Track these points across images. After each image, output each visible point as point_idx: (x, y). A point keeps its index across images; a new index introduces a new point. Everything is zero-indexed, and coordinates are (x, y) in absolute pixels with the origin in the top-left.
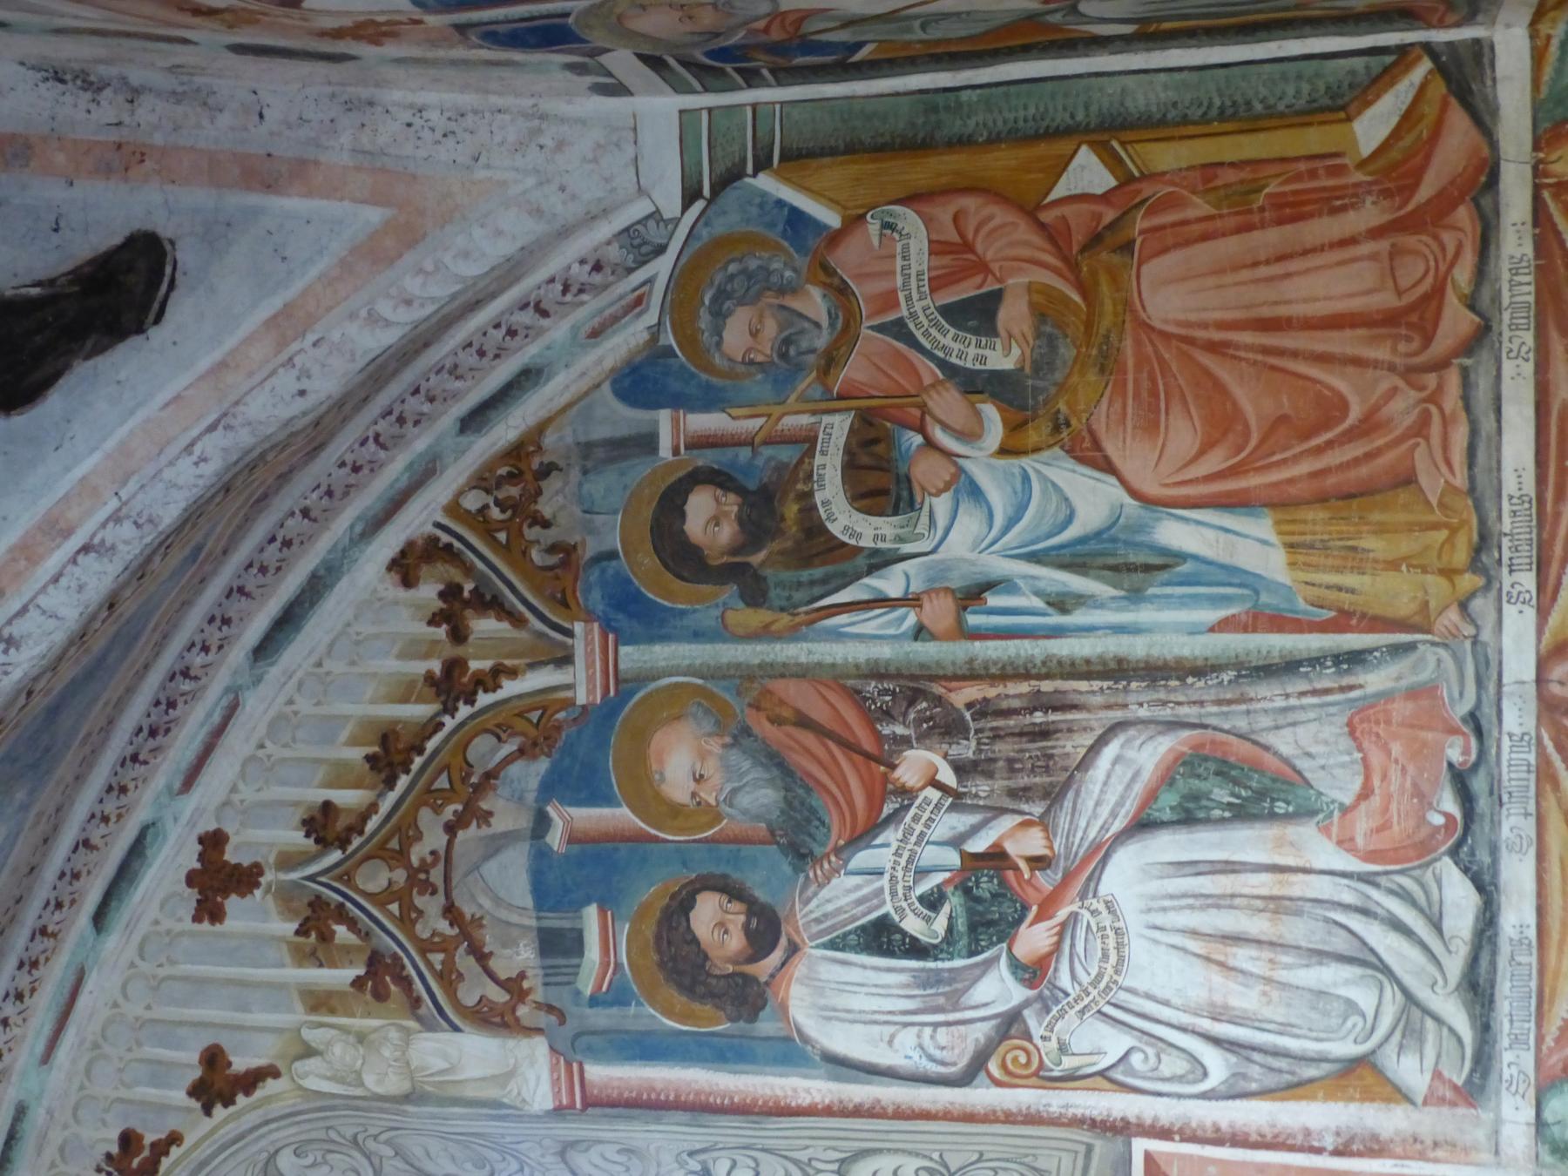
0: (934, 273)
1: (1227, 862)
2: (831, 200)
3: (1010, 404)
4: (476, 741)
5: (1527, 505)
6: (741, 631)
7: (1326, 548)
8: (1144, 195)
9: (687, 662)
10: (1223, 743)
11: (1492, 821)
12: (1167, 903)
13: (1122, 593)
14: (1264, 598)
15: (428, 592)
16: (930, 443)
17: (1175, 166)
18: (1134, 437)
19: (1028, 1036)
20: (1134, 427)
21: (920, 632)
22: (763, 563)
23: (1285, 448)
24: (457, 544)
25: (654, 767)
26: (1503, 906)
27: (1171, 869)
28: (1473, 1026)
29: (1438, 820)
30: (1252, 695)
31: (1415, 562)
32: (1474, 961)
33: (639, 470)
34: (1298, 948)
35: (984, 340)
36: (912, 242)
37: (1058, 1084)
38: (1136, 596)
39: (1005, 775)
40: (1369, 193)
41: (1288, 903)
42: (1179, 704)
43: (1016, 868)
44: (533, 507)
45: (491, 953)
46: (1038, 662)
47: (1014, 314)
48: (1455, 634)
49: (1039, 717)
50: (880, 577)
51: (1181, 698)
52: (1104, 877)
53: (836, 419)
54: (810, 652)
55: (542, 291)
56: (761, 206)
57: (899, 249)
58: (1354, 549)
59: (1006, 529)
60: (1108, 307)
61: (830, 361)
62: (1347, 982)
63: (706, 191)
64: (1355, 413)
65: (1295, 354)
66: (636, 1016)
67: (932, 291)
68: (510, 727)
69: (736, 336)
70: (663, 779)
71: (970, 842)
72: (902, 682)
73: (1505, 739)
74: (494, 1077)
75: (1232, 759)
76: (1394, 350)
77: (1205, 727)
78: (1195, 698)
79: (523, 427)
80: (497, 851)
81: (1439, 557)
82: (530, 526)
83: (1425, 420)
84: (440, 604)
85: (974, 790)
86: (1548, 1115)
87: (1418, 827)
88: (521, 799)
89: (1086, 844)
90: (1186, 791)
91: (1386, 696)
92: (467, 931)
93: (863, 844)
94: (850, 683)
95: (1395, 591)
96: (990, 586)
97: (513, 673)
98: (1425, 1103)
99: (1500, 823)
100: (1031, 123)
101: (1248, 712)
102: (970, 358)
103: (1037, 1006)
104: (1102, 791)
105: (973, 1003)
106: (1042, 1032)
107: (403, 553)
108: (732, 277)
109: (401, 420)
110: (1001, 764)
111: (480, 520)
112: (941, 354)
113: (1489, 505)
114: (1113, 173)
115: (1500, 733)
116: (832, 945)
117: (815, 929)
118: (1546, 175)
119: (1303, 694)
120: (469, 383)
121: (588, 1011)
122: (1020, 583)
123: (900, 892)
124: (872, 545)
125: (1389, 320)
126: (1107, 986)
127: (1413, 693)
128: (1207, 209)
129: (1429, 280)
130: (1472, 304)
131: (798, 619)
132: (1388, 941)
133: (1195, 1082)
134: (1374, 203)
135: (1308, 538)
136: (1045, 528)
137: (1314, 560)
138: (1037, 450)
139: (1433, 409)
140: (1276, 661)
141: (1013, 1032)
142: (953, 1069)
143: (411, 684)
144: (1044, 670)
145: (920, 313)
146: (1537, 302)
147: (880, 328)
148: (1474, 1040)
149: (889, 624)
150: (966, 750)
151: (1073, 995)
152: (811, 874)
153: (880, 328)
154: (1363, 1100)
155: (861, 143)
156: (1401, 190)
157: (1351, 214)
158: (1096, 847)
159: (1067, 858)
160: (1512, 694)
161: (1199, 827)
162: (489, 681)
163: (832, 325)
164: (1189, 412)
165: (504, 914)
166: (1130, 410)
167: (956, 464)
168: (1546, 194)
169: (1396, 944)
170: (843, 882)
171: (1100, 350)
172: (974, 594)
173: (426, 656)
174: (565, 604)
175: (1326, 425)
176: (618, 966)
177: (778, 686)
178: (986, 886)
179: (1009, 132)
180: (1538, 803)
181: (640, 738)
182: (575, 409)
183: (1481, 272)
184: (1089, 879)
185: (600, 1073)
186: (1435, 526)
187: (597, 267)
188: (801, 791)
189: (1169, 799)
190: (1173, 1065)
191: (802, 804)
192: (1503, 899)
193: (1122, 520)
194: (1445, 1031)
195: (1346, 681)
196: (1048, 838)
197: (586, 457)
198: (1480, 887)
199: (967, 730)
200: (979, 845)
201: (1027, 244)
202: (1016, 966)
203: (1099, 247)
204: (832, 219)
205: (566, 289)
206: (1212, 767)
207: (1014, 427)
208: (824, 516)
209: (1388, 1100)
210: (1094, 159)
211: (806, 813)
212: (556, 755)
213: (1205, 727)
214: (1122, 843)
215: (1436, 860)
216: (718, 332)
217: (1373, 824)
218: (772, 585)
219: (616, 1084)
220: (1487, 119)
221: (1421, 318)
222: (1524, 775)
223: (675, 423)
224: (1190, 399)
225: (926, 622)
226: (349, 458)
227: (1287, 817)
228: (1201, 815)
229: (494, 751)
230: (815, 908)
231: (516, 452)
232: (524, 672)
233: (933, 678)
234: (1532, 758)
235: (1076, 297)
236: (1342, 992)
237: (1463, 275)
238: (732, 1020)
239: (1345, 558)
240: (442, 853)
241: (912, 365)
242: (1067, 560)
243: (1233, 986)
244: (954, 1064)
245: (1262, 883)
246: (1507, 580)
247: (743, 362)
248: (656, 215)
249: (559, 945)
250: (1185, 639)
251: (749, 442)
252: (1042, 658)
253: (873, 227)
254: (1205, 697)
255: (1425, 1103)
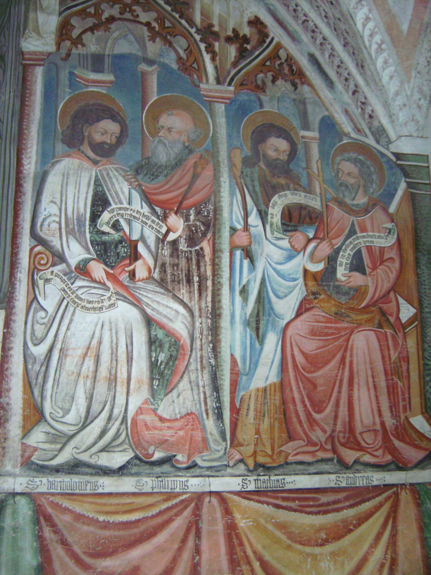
0: (373, 248)
1: (132, 358)
2: (398, 210)
3: (324, 275)
4: (185, 41)
5: (281, 486)
6: (232, 155)
7: (264, 404)
8: (399, 334)
9: (218, 130)
10: (184, 359)
11: (150, 473)
12: (114, 331)
13: (248, 318)
14: (244, 378)
15: (246, 31)
16: (309, 241)
17: (408, 346)
18: (309, 325)
19: (54, 265)
20: (314, 326)
21: (233, 230)
22: (260, 167)
23: (304, 388)
24: (265, 45)
25: (174, 112)
26: (112, 478)
27: (129, 334)
28: (58, 465)
29: (151, 451)
30: (204, 372)
31: (259, 441)
32: (89, 466)
33: (296, 123)
34: (94, 388)
35: (348, 266)
36: (384, 240)
37: (30, 277)
38: (247, 323)
39: (171, 262)
40: (397, 422)
41: (114, 385)
42: (201, 340)
43: (130, 264)
44: (280, 77)
45: (93, 33)
46: (219, 280)
47: (358, 279)
48: (230, 457)
49: (196, 279)
50: (256, 215)
51: (203, 341)
52: (125, 304)
53: (319, 203)
54: (225, 182)
55: (361, 94)
56: (394, 182)
57: (382, 235)
58: (264, 416)
59: (274, 269)
60: (359, 317)
61: (341, 204)
62: (78, 410)
63: (399, 162)
64: (317, 416)
65: (339, 392)
66: (64, 91)
67: (367, 247)
68: (191, 54)
69: (348, 167)
70: (169, 115)
71: (142, 245)
72: (213, 220)
73: (186, 479)
74: (38, 27)
75: (177, 362)
76: (340, 432)
77: (191, 351)
78: (204, 347)
79: (311, 78)
80: (138, 42)
81: (261, 451)
82: (273, 75)
83: (315, 445)
84: (241, 35)
85: (165, 248)
86: (18, 498)
87: (148, 442)
88: (161, 55)
89: (140, 296)
90: (164, 342)
91: (204, 429)
92: (103, 24)
93: (143, 197)
94: (213, 198)
95: (246, 434)
96: (252, 261)
97: (213, 59)
98: (23, 443)
99: (149, 477)
100: (424, 291)
101: (197, 370)
102: (342, 260)
103: (67, 270)
104: (164, 305)
105: (69, 241)
106: (55, 271)
107: (262, 23)
108: (369, 168)
109: (313, 31)
110: (176, 261)
111: (275, 56)
112: (343, 248)
113: (281, 471)
114: (407, 321)
115: (188, 477)
116: (97, 180)
117: (104, 173)
118: (401, 489)
119: (205, 393)
120: (328, 60)
121: (67, 71)
122: (253, 274)
123: (121, 212)
124: (270, 213)
125: (351, 430)
126: (76, 302)
127: (205, 440)
128: (393, 359)
129: (365, 445)
130: (356, 462)
131: (238, 178)
132: (96, 428)
133: (32, 340)
134: (393, 423)
135: (268, 397)
136: (275, 286)
137: (260, 398)
138: (306, 285)
139: (318, 448)
140: (219, 382)
141: (56, 258)
142: (39, 230)
143: (208, 17)
144: (216, 282)
145: (359, 241)
146: (357, 487)
147: (353, 225)
148: (51, 466)
149: (237, 217)
150: (183, 246)
151: (72, 287)
152: (129, 173)
153: (353, 225)
154: (24, 416)
155: (418, 224)
156: (397, 433)
157: (389, 415)
158: (139, 300)
159: (134, 287)
160: (205, 481)
161: (147, 347)
162: (210, 49)
163: (354, 205)
164: (319, 349)
165: (110, 42)
166: (320, 324)
167: (301, 250)
168: (395, 489)
169: (95, 432)
170: (126, 187)
171: (344, 313)
172: (248, 254)
173: (220, 26)
174: (242, 84)
175: (313, 405)
176: (87, 86)
177: (210, 167)
178: (122, 251)
179: (421, 282)
180: (157, 493)
181: (187, 107)
182: (318, 100)
183: (367, 465)
184: (125, 297)
185: (39, 76)
186: (273, 449)
187: (371, 117)
188: (165, 172)
189: (160, 334)
190: (40, 330)
191: (160, 173)
192: (116, 478)
193: (277, 319)
194: (56, 453)
195: (210, 412)
196: (143, 280)
197: (300, 102)
198: (121, 469)
199: (191, 247)
200: (141, 248)
201: (382, 286)
202: (86, 262)
203: (380, 315)
204: (392, 209)
205: (363, 103)
206: (174, 354)
207: (315, 276)
208: (281, 194)
209: (24, 427)
210: (411, 314)
211: (156, 174)
212: (179, 72)
213: (191, 351)
214: (140, 312)
215: (133, 450)
216: (349, 160)
217: (149, 423)
218: (252, 169)
219: (34, 79)
220: (421, 466)
221: (352, 442)
222: (170, 487)
223: (314, 139)
224: (324, 349)
225: (238, 233)
226: (299, 8)
227: (151, 385)
228: (153, 348)
229: (181, 47)
230: (114, 174)
231: (301, 74)
232: (214, 64)
233: (214, 234)
234: (178, 490)
235: (363, 305)
236: (74, 408)
237: (367, 458)
238: (63, 132)
239: (260, 412)
240: (137, 19)
241: (339, 236)
242: (262, 295)
243: (76, 359)
244: (41, 230)
245: (122, 374)
246: (252, 478)
247: (338, 169)
248: (389, 142)
249: (97, 62)
250: (228, 344)
251: (308, 167)
252: (221, 282)
253: (389, 225)
254: (204, 351)
255: (23, 443)
